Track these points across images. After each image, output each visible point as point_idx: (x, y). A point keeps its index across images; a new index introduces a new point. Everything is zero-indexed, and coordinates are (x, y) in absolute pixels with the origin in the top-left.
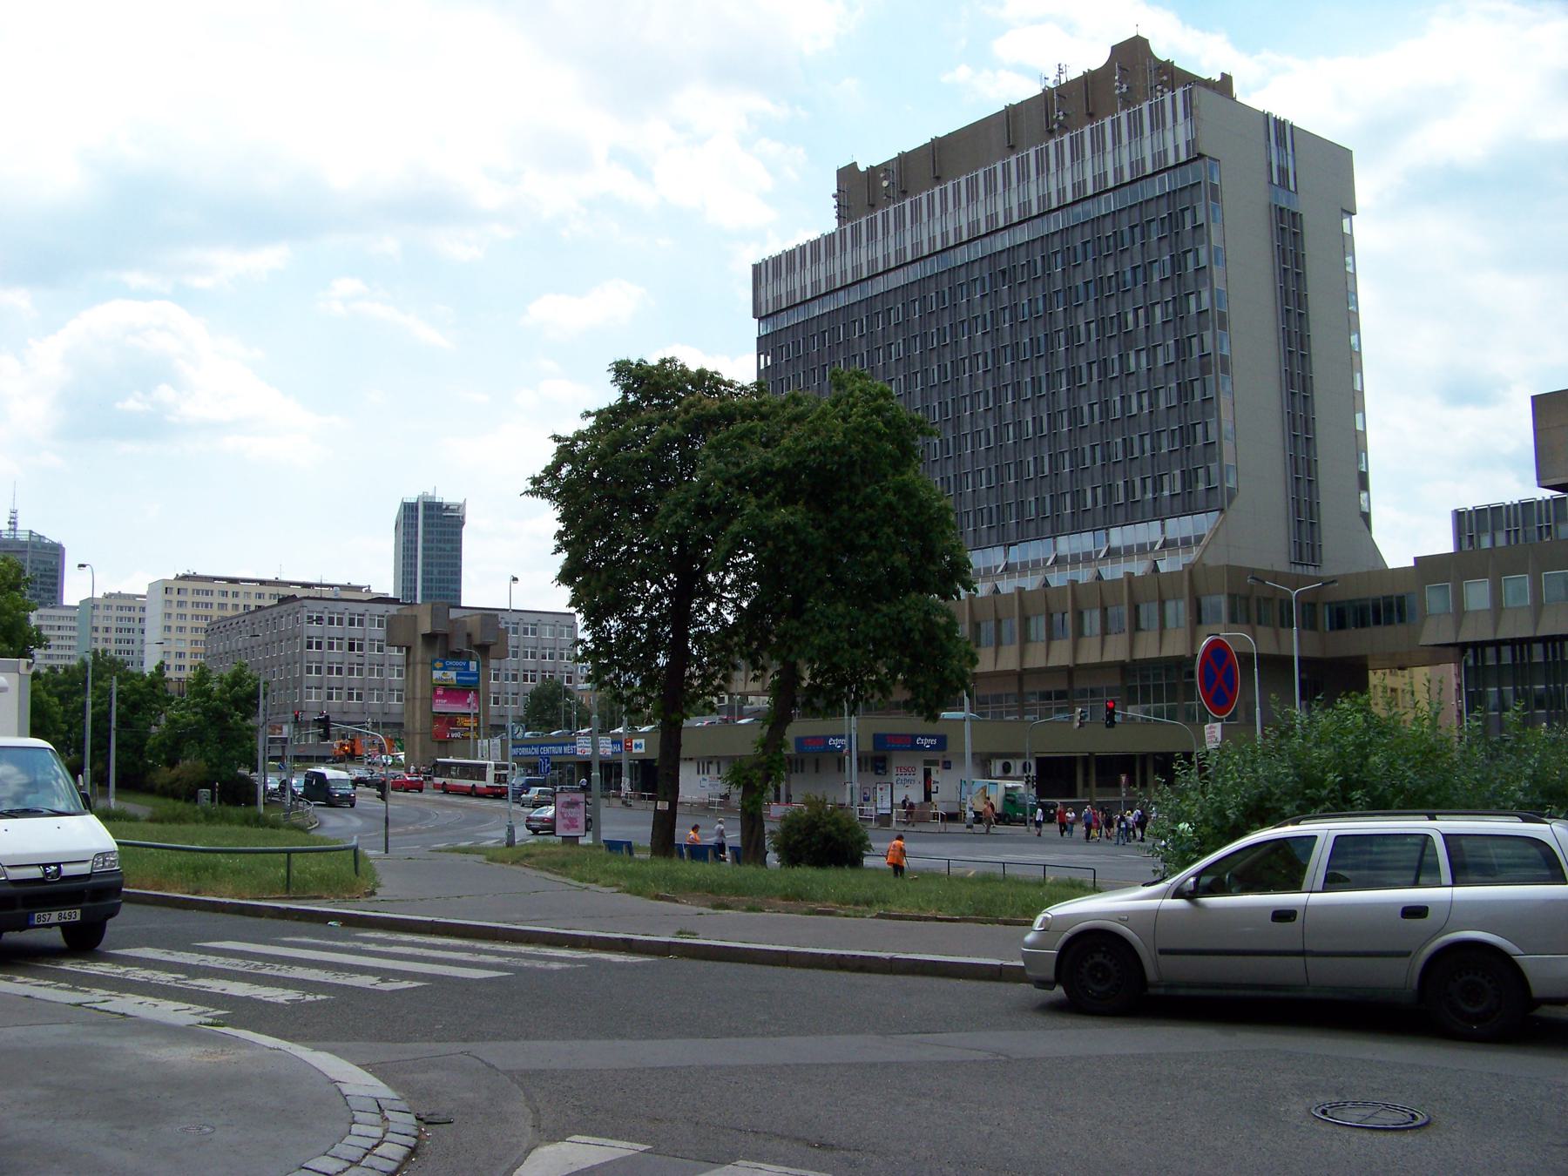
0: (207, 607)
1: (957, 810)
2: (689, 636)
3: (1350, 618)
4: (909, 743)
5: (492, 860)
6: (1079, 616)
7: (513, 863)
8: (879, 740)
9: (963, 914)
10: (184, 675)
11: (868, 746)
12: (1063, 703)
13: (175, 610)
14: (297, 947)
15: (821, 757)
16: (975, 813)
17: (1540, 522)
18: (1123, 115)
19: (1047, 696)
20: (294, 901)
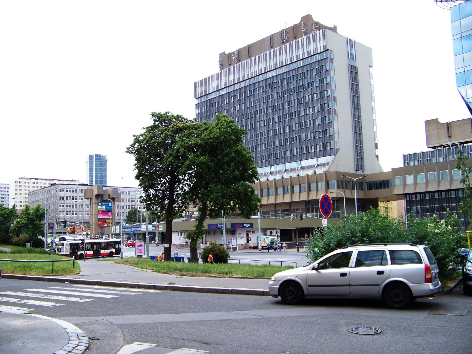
0: (28, 187)
1: (257, 246)
2: (174, 195)
3: (373, 187)
4: (242, 226)
5: (116, 263)
6: (292, 187)
7: (122, 264)
8: (233, 225)
9: (254, 276)
10: (21, 208)
11: (229, 227)
12: (288, 213)
13: (18, 188)
14: (55, 290)
15: (215, 230)
16: (262, 246)
17: (427, 158)
18: (305, 37)
19: (283, 211)
20: (55, 276)
